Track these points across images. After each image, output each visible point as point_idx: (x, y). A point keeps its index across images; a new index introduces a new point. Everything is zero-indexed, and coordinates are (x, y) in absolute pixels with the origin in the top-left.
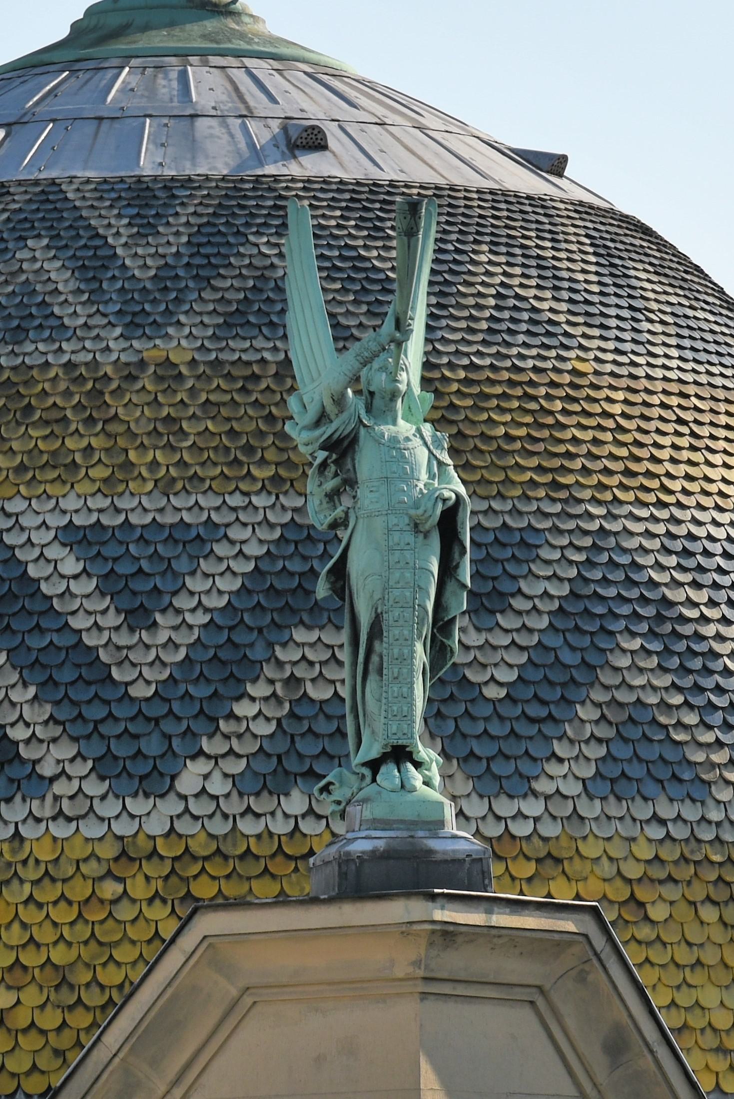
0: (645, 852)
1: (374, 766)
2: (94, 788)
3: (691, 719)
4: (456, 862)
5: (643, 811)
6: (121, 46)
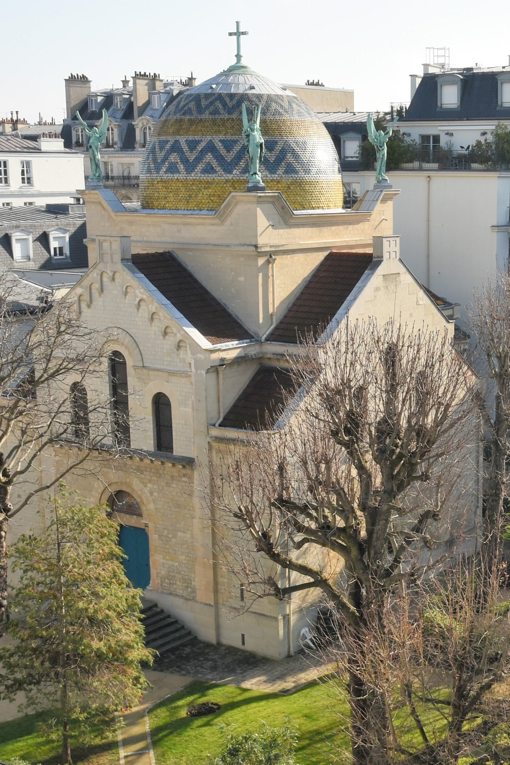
0: (290, 181)
1: (252, 175)
2: (223, 173)
3: (296, 164)
4: (261, 187)
5: (290, 176)
6: (231, 73)
